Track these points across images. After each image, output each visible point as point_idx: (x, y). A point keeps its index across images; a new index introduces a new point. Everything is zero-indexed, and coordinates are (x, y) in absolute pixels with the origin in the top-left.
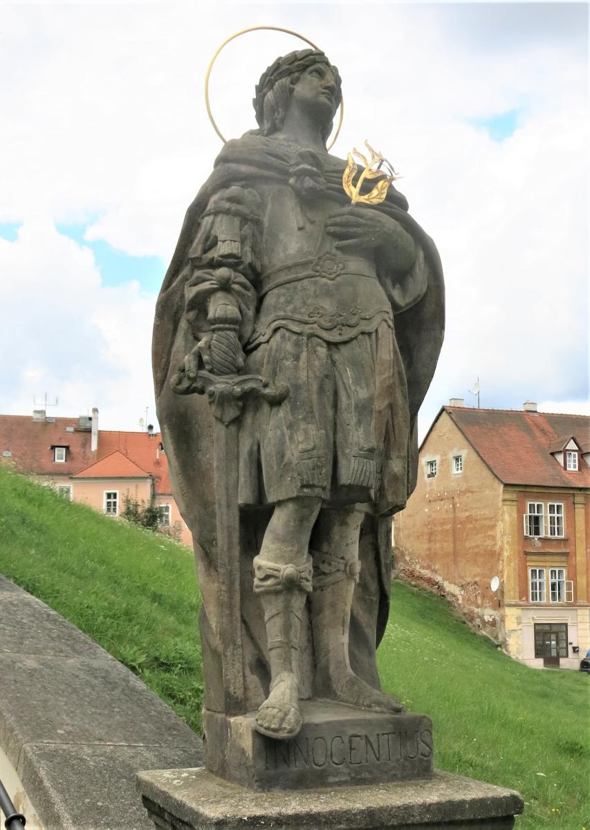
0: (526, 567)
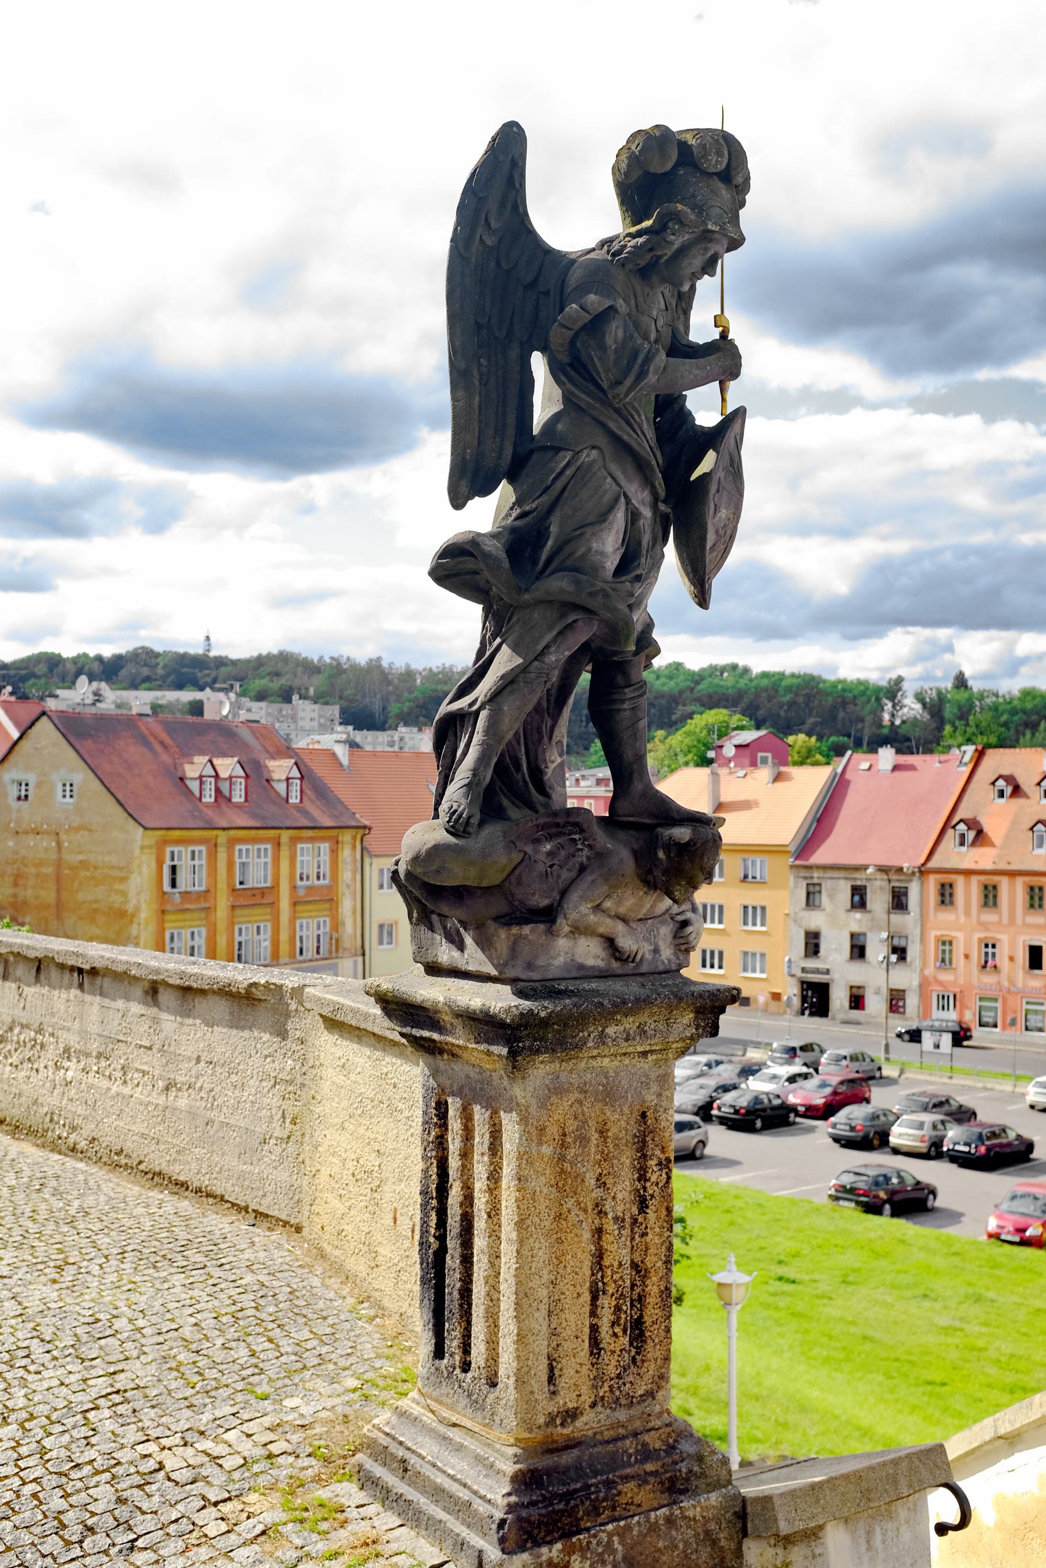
0: (164, 929)
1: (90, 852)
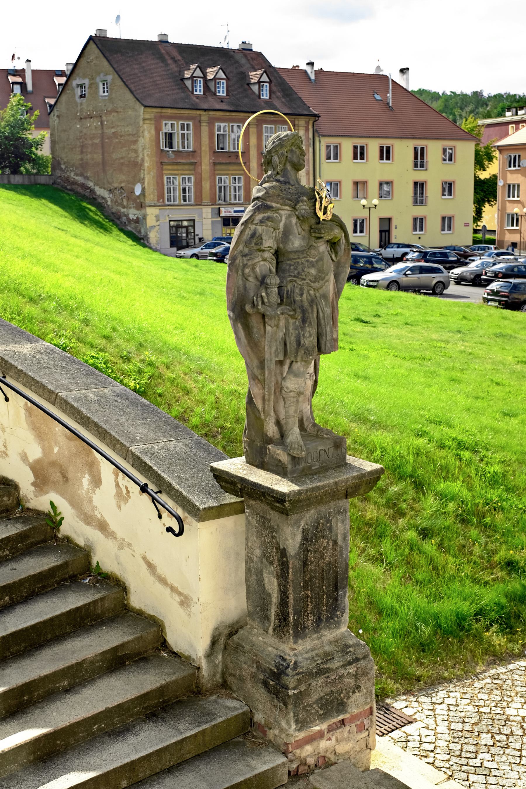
0: (163, 175)
1: (118, 126)
